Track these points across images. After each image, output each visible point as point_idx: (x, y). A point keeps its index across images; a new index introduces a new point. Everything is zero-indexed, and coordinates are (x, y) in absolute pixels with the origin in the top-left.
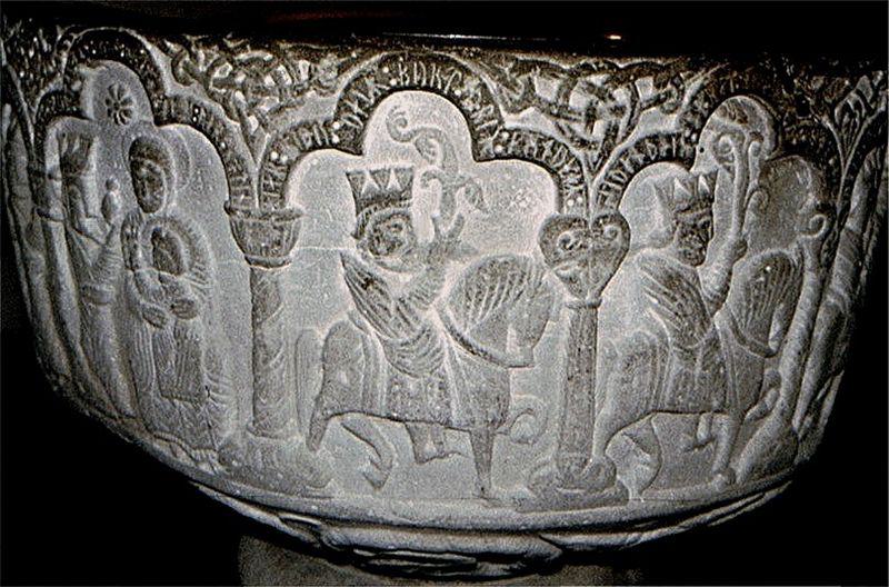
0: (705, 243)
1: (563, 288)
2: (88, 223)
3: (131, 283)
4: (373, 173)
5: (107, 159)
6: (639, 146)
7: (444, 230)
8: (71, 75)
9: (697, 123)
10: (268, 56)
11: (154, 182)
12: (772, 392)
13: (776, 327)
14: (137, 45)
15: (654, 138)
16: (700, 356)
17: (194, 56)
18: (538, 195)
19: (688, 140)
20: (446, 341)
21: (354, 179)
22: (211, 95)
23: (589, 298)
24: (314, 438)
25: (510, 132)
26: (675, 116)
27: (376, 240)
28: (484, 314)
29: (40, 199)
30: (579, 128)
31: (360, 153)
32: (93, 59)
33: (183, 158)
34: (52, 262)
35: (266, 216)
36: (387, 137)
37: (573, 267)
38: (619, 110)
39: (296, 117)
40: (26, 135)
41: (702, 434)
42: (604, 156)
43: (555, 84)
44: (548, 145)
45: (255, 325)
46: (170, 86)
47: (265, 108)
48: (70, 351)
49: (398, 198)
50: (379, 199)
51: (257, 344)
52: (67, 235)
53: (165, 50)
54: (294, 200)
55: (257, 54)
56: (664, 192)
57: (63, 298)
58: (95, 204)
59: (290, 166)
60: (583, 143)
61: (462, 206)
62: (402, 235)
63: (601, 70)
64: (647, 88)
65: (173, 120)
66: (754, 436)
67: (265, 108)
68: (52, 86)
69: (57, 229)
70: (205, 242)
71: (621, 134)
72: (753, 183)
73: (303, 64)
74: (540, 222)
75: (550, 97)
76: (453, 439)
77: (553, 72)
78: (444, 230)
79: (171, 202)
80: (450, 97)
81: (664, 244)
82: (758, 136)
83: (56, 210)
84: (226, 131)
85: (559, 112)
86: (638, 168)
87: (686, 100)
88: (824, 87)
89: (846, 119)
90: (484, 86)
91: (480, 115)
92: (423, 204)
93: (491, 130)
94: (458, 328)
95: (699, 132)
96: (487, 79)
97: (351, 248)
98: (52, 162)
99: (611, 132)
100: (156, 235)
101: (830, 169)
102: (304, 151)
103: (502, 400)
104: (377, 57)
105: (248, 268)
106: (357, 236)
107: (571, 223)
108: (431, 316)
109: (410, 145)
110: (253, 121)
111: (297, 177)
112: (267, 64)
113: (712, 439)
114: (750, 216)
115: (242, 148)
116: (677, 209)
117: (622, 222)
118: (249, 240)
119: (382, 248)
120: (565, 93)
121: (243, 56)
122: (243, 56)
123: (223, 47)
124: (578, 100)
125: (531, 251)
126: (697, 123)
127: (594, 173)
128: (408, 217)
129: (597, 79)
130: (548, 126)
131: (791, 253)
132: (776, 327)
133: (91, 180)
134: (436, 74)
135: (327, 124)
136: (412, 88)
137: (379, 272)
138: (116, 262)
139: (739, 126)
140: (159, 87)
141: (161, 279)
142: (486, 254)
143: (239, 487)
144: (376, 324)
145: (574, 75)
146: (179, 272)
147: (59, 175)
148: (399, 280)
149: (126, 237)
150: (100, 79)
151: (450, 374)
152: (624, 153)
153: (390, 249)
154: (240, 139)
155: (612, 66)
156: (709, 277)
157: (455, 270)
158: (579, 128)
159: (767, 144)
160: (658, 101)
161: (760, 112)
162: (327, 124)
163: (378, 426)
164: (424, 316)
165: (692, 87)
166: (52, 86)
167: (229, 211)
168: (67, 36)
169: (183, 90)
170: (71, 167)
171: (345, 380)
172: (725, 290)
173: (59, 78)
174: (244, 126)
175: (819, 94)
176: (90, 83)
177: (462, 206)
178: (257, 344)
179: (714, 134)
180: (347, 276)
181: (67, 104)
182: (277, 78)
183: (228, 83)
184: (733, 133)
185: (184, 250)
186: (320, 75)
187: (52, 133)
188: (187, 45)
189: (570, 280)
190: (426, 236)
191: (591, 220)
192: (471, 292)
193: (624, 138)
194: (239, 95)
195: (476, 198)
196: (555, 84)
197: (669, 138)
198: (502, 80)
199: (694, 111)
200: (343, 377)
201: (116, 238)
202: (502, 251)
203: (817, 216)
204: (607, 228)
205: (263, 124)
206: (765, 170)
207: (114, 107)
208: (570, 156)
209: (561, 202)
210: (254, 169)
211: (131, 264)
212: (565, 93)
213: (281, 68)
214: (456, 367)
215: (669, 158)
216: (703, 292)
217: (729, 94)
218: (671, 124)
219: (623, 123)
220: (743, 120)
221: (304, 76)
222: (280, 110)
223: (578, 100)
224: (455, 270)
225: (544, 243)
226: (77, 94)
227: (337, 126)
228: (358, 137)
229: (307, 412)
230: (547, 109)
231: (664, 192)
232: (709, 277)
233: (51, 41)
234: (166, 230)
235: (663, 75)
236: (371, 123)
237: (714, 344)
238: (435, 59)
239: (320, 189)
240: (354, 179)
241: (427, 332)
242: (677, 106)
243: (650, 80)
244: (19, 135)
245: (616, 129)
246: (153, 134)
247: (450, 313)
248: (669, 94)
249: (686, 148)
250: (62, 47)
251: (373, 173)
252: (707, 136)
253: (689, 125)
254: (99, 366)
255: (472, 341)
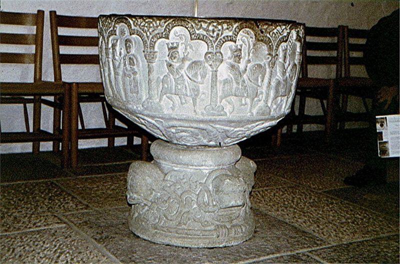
0: (240, 59)
1: (209, 67)
2: (117, 58)
3: (125, 70)
4: (171, 43)
5: (121, 44)
6: (224, 38)
7: (185, 55)
8: (114, 27)
9: (236, 34)
10: (151, 20)
11: (130, 47)
12: (261, 95)
13: (260, 80)
14: (128, 19)
15: (227, 36)
16: (240, 83)
17: (138, 21)
18: (203, 47)
19: (235, 37)
20: (186, 78)
21: (168, 44)
22: (141, 29)
23: (215, 69)
24: (160, 100)
25: (197, 34)
26: (232, 32)
27: (172, 57)
28: (193, 72)
29: (107, 54)
30: (211, 34)
31: (168, 39)
32: (118, 23)
33: (135, 43)
34: (109, 69)
35: (151, 52)
36: (174, 36)
37: (211, 62)
38: (219, 30)
39: (156, 32)
40: (105, 41)
41: (243, 102)
42: (217, 39)
43: (206, 25)
44: (205, 37)
45: (149, 76)
46: (133, 27)
47: (151, 30)
48: (112, 89)
49: (176, 48)
50: (172, 48)
51: (149, 79)
52: (112, 60)
53: (132, 20)
54: (156, 49)
55: (150, 20)
56: (230, 48)
57: (111, 76)
58: (118, 53)
59: (155, 42)
60: (212, 37)
61: (189, 50)
62: (177, 55)
63: (215, 22)
64: (225, 26)
65: (133, 34)
66: (395, 234)
67: (151, 30)
68: (111, 29)
69: (110, 60)
70: (139, 59)
71: (220, 35)
72: (251, 47)
73: (158, 22)
74: (205, 53)
75: (205, 27)
76: (188, 98)
77: (206, 22)
78: (185, 55)
79: (133, 51)
80: (186, 27)
81: (231, 59)
82: (251, 38)
83: (110, 56)
84: (143, 35)
85: (207, 30)
86: (224, 42)
87: (234, 29)
88: (267, 28)
89: (274, 35)
90: (192, 25)
91: (191, 31)
92: (181, 49)
93: (193, 34)
94: (188, 75)
95: (237, 36)
96: (193, 24)
97: (167, 58)
98: (110, 45)
99: (218, 35)
100: (130, 58)
101: (270, 46)
102: (158, 39)
103: (198, 90)
104: (172, 20)
105: (147, 64)
106: (168, 56)
107: (210, 53)
108: (183, 72)
109: (178, 38)
110: (148, 33)
111: (157, 44)
112: (151, 22)
113: (246, 104)
114: (251, 55)
115: (146, 39)
116: (233, 51)
117: (221, 53)
118: (148, 58)
119: (173, 58)
120: (208, 27)
121: (147, 21)
122: (147, 21)
123: (143, 19)
124: (211, 28)
125: (203, 59)
126: (236, 34)
127: (214, 43)
128: (178, 52)
129: (215, 24)
130: (205, 33)
131: (262, 63)
132: (260, 80)
133: (118, 48)
134: (183, 23)
135: (162, 33)
136: (178, 26)
137: (172, 63)
138: (122, 65)
139: (247, 35)
140: (131, 27)
141: (131, 67)
142: (194, 60)
143: (146, 112)
144: (172, 74)
145: (210, 23)
146: (134, 65)
147: (111, 48)
148: (176, 65)
149: (124, 60)
150: (120, 27)
151: (187, 85)
152: (221, 39)
153: (174, 58)
154: (146, 37)
155: (218, 22)
156: (242, 66)
157: (187, 63)
158: (211, 34)
159: (254, 39)
160: (228, 29)
161: (252, 32)
162: (162, 33)
163: (173, 96)
164: (182, 73)
165: (235, 26)
166: (111, 29)
167: (144, 52)
168: (114, 19)
169: (136, 28)
170: (114, 46)
171: (166, 87)
172: (246, 70)
173: (112, 28)
174: (146, 34)
175: (266, 30)
176: (118, 28)
177: (189, 50)
178: (149, 79)
179: (241, 37)
180: (167, 65)
181: (113, 33)
182: (153, 25)
183: (144, 26)
184: (246, 37)
185: (135, 61)
186: (161, 23)
187: (110, 39)
188: (136, 19)
189: (211, 65)
190: (182, 56)
191: (214, 53)
192: (190, 67)
193: (221, 36)
194: (146, 28)
195: (191, 47)
196: (206, 25)
197: (230, 36)
198: (196, 24)
199: (236, 31)
200: (166, 86)
201: (122, 60)
202: (197, 59)
203: (268, 56)
204: (218, 54)
205: (151, 34)
206: (254, 45)
207: (122, 33)
208: (209, 39)
209: (208, 49)
210: (149, 43)
211: (125, 65)
212: (208, 27)
213: (154, 23)
214: (188, 83)
215: (231, 40)
216: (241, 70)
217: (243, 28)
218: (231, 34)
219: (220, 33)
220: (248, 34)
221: (158, 24)
222: (153, 31)
223: (211, 28)
224: (187, 63)
225: (205, 57)
226: (115, 31)
227: (164, 33)
228: (168, 35)
229: (159, 94)
230: (204, 30)
231: (230, 48)
232: (242, 66)
233: (111, 21)
234: (131, 57)
235: (229, 24)
236: (171, 33)
237: (244, 81)
238: (183, 20)
239: (161, 46)
240: (168, 44)
241: (182, 76)
242: (231, 30)
243: (226, 25)
244: (104, 42)
245: (219, 34)
246: (130, 37)
247: (187, 72)
248: (230, 27)
249: (234, 39)
250: (113, 21)
251: (171, 43)
252: (239, 37)
253: (235, 34)
254: (119, 92)
255: (191, 78)
